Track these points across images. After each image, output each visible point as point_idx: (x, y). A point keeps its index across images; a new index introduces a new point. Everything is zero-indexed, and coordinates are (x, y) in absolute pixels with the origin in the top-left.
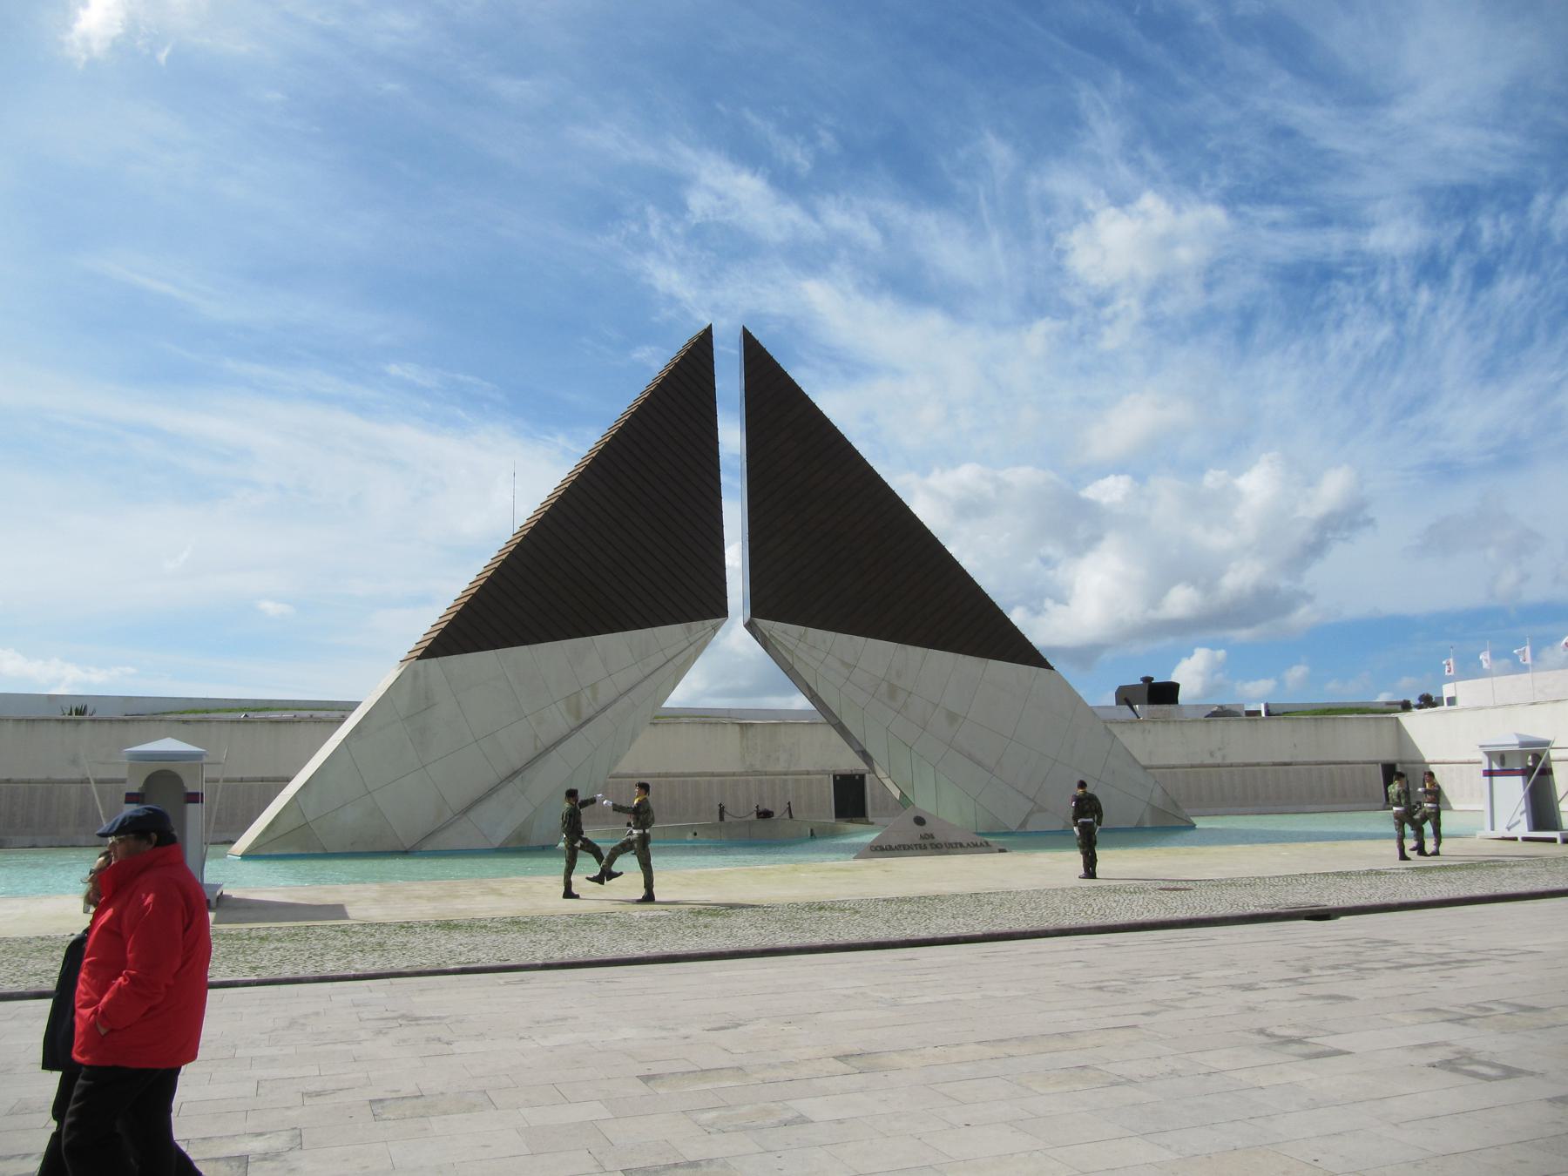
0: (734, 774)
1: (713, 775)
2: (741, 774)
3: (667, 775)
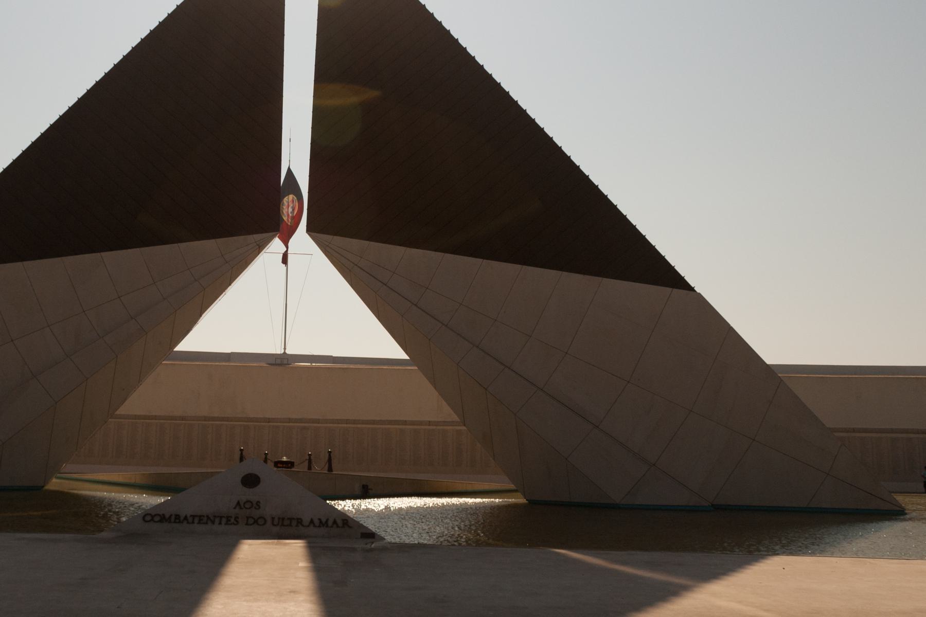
0: (429, 423)
1: (405, 423)
2: (437, 423)
3: (355, 422)
